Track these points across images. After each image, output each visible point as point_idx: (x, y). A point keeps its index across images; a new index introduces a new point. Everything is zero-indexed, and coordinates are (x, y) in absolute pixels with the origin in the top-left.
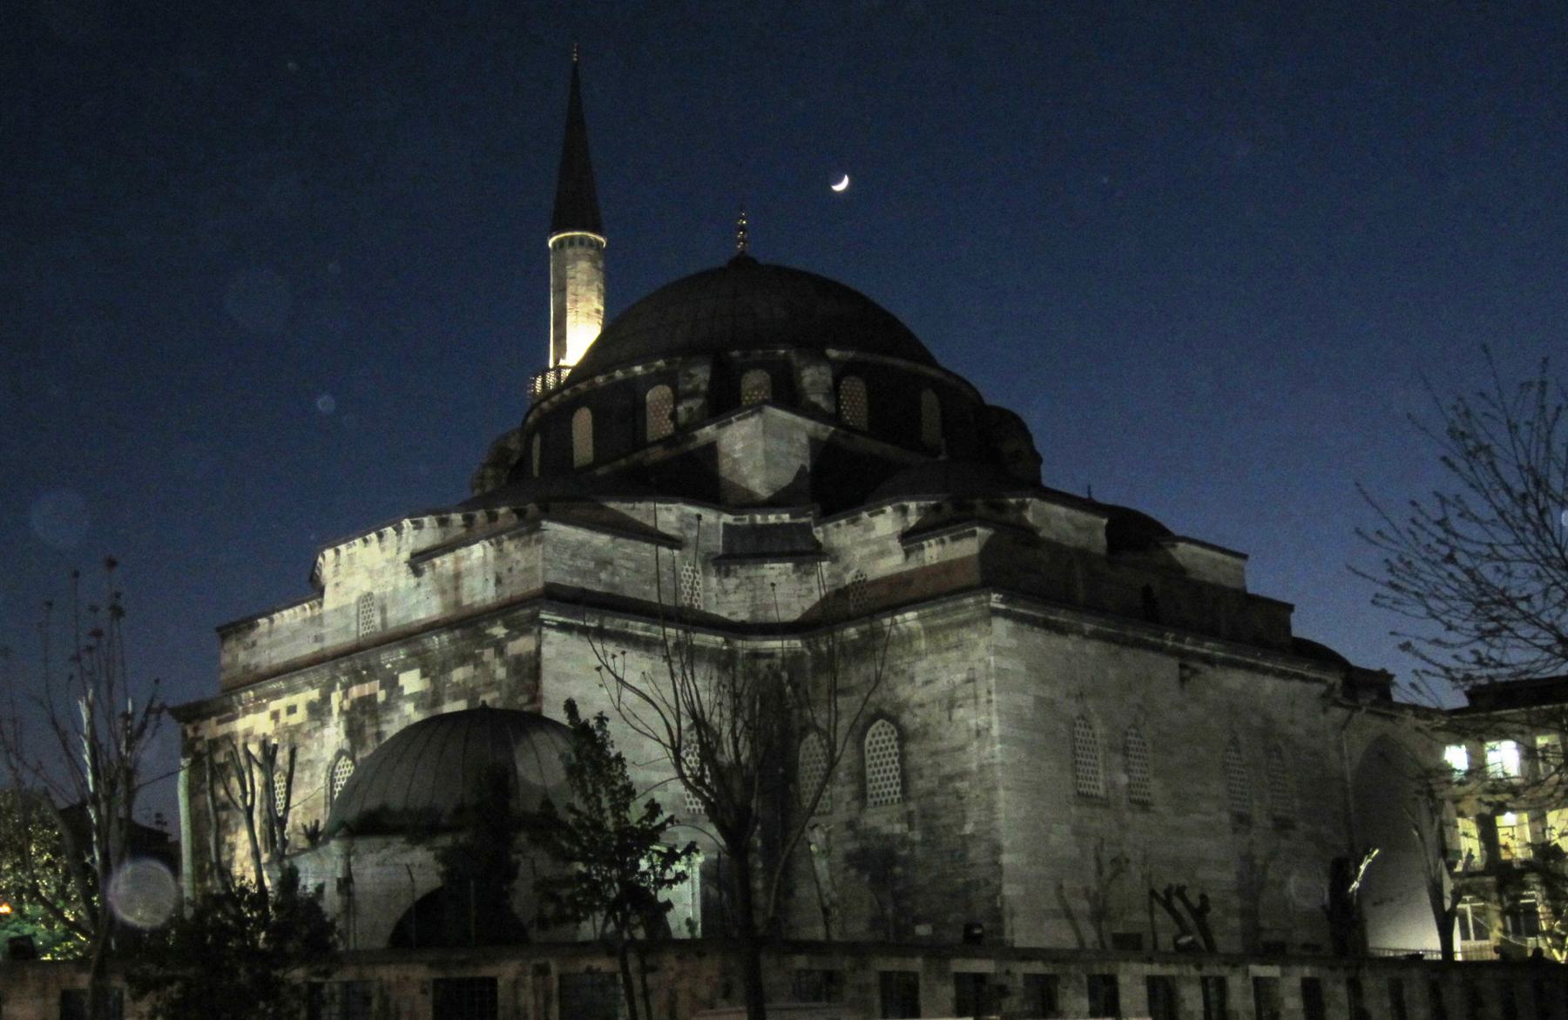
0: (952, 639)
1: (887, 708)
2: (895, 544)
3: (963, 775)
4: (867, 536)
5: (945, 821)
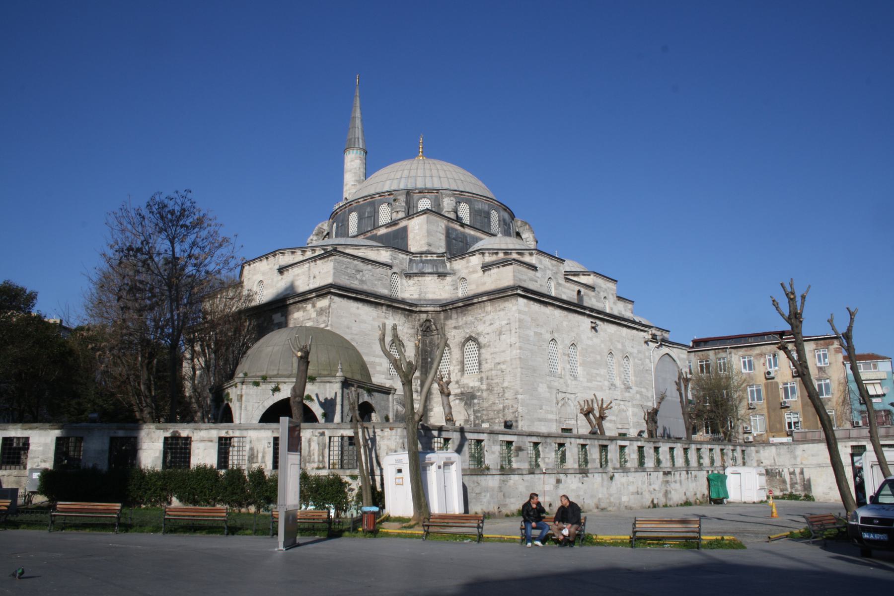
0: (502, 307)
1: (474, 335)
3: (504, 363)
5: (496, 381)
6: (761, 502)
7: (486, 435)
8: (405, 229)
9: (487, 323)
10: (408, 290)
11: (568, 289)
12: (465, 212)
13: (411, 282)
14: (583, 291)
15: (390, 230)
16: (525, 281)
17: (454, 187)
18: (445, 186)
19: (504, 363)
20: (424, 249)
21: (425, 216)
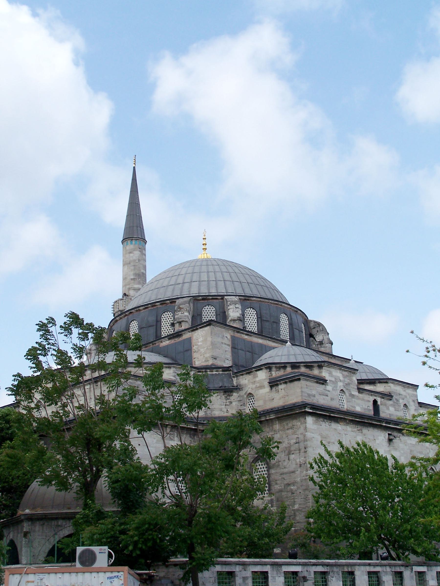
0: (290, 425)
2: (266, 384)
3: (294, 484)
4: (254, 380)
6: (13, 574)
7: (269, 567)
8: (190, 339)
11: (363, 400)
12: (252, 323)
14: (379, 400)
15: (173, 341)
17: (240, 291)
18: (231, 290)
19: (294, 484)
20: (210, 363)
21: (208, 328)
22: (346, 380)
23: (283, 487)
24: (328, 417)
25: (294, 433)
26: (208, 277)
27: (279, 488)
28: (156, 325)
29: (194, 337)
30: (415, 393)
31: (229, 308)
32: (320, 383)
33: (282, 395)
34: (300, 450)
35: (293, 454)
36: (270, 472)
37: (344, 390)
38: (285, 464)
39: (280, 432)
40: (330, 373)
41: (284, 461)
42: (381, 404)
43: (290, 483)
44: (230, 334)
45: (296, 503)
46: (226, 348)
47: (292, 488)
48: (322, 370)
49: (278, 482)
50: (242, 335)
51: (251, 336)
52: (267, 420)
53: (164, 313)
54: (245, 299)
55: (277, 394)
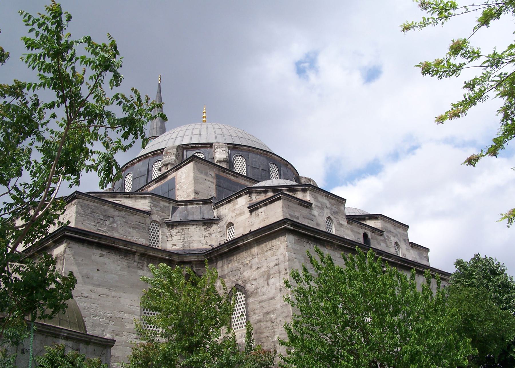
1: (240, 283)
2: (247, 210)
3: (273, 312)
5: (265, 334)
8: (174, 179)
9: (254, 267)
10: (173, 241)
13: (174, 231)
15: (159, 184)
16: (298, 218)
19: (273, 312)
22: (333, 208)
23: (262, 316)
24: (312, 239)
25: (273, 255)
26: (200, 131)
27: (257, 318)
28: (148, 175)
29: (178, 176)
30: (406, 233)
31: (216, 151)
32: (304, 206)
33: (262, 218)
34: (280, 272)
35: (272, 278)
36: (248, 302)
37: (332, 217)
38: (264, 290)
39: (259, 256)
40: (316, 198)
41: (263, 287)
42: (372, 239)
43: (269, 311)
44: (214, 172)
45: (276, 333)
46: (210, 184)
47: (272, 316)
48: (306, 194)
49: (256, 311)
50: (228, 175)
51: (237, 177)
52: (244, 244)
53: (156, 162)
54: (234, 148)
55: (257, 218)
